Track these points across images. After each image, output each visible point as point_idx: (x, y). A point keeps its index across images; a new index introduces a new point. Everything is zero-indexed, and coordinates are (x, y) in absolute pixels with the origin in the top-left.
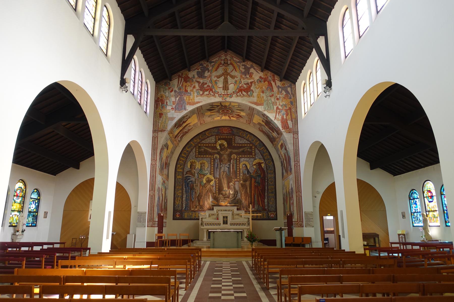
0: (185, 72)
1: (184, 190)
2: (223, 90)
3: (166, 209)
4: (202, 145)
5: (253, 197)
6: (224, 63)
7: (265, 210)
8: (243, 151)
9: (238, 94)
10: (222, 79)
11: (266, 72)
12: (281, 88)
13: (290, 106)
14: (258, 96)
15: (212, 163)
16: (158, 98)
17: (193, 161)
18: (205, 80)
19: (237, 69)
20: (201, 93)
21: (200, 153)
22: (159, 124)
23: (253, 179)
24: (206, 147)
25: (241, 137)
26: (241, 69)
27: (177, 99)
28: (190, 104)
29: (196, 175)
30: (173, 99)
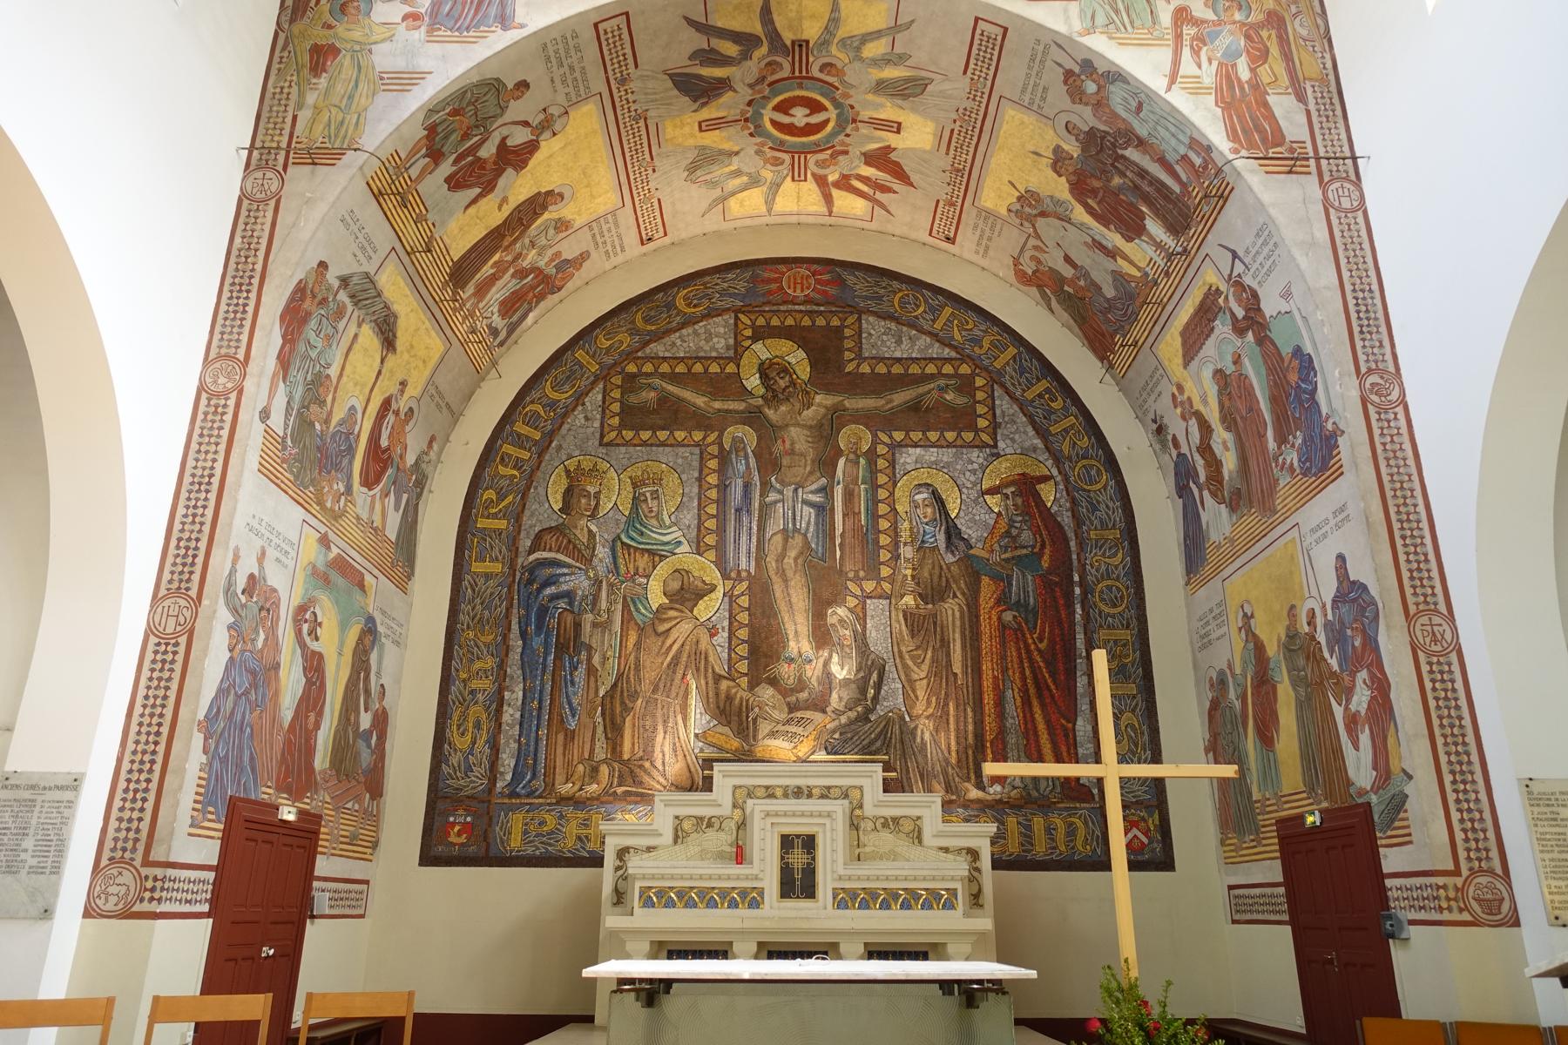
1: (515, 656)
4: (648, 368)
5: (988, 699)
8: (915, 407)
15: (713, 479)
21: (633, 417)
22: (304, 116)
23: (985, 580)
24: (673, 378)
29: (602, 552)
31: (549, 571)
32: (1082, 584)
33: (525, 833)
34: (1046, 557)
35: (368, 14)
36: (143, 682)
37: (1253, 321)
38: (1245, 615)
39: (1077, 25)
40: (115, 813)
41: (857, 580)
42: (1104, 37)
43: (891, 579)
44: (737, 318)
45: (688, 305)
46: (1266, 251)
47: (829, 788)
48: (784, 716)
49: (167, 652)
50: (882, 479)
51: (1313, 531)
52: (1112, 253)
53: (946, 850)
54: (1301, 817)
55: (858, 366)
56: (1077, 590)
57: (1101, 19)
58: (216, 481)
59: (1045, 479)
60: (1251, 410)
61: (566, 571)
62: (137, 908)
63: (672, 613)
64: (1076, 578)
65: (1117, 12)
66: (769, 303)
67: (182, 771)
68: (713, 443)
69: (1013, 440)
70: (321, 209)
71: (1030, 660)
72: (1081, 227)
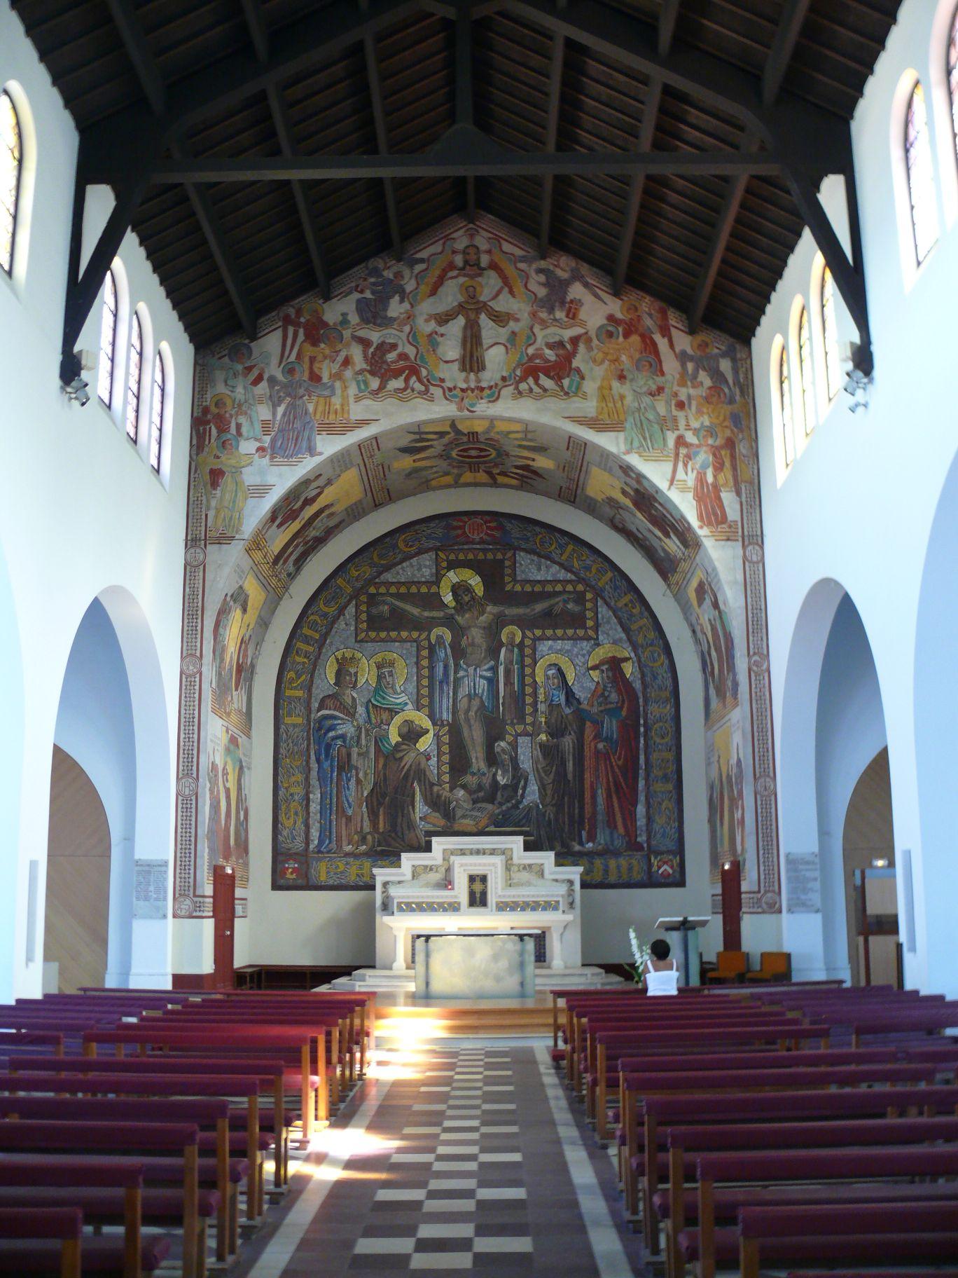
0: (307, 303)
1: (314, 774)
3: (243, 847)
6: (466, 262)
7: (639, 847)
8: (548, 614)
9: (523, 386)
11: (633, 296)
12: (691, 359)
13: (728, 433)
15: (425, 663)
16: (206, 410)
18: (390, 335)
19: (519, 286)
20: (375, 383)
21: (375, 623)
22: (211, 514)
23: (588, 724)
24: (398, 596)
25: (539, 556)
26: (533, 286)
27: (281, 410)
28: (331, 429)
29: (361, 710)
30: (263, 412)
31: (331, 722)
32: (645, 725)
39: (623, 448)
41: (512, 724)
42: (636, 456)
43: (533, 724)
48: (470, 806)
49: (187, 804)
50: (528, 661)
52: (660, 539)
53: (556, 881)
56: (642, 729)
57: (636, 444)
58: (196, 720)
59: (626, 660)
65: (645, 439)
66: (457, 543)
67: (203, 857)
70: (227, 570)
71: (613, 772)
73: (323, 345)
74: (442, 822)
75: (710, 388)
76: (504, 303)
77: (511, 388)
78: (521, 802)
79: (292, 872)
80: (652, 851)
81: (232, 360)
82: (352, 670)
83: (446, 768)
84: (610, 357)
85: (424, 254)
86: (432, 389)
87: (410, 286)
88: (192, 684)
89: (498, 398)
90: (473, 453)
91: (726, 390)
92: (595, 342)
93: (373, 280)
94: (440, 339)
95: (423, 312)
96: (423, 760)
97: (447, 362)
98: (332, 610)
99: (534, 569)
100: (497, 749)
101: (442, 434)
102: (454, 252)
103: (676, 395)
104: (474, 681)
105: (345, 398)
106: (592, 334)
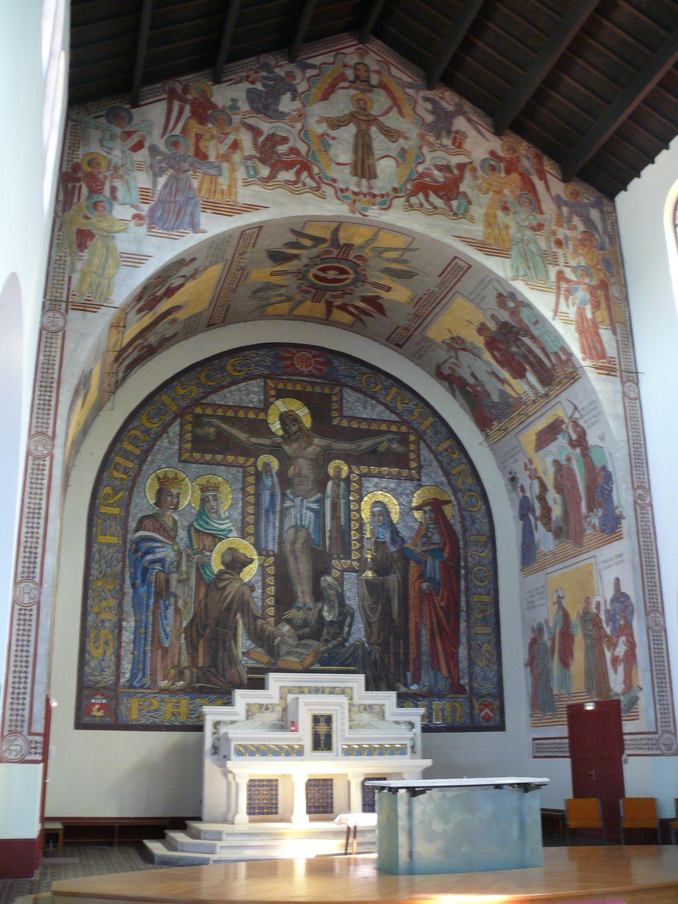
0: (197, 83)
1: (128, 600)
2: (355, 175)
4: (209, 411)
6: (357, 77)
7: (460, 690)
8: (373, 451)
9: (414, 200)
10: (349, 132)
11: (512, 138)
12: (566, 204)
13: (602, 276)
14: (490, 222)
15: (251, 489)
16: (76, 168)
17: (171, 475)
18: (281, 128)
19: (407, 109)
20: (265, 171)
21: (200, 444)
22: (76, 277)
23: (412, 563)
24: (225, 419)
25: (365, 394)
26: (420, 110)
27: (162, 181)
28: (217, 209)
29: (182, 534)
30: (143, 180)
33: (140, 710)
34: (447, 551)
35: (110, 212)
36: (14, 632)
37: (580, 442)
38: (559, 596)
40: (8, 706)
43: (358, 560)
44: (266, 383)
45: (235, 370)
46: (593, 413)
47: (334, 688)
51: (605, 562)
52: (503, 381)
53: (397, 723)
54: (582, 706)
55: (341, 421)
56: (463, 572)
57: (521, 273)
58: (43, 512)
59: (448, 502)
60: (573, 487)
61: (159, 545)
62: (28, 758)
63: (227, 576)
64: (462, 564)
65: (529, 268)
66: (285, 374)
68: (251, 466)
69: (430, 477)
71: (437, 614)
72: (487, 363)
73: (210, 125)
74: (266, 658)
75: (584, 232)
76: (393, 121)
77: (403, 199)
78: (346, 640)
79: (100, 708)
80: (474, 694)
81: (109, 122)
82: (174, 491)
83: (271, 601)
84: (493, 188)
85: (316, 61)
86: (324, 188)
87: (302, 87)
88: (40, 468)
89: (390, 207)
90: (331, 274)
91: (597, 237)
92: (480, 173)
93: (264, 74)
94: (331, 142)
95: (314, 112)
96: (247, 592)
97: (339, 164)
98: (155, 426)
99: (360, 408)
100: (323, 584)
101: (318, 240)
102: (345, 66)
103: (554, 233)
104: (301, 512)
105: (233, 181)
106: (477, 164)
